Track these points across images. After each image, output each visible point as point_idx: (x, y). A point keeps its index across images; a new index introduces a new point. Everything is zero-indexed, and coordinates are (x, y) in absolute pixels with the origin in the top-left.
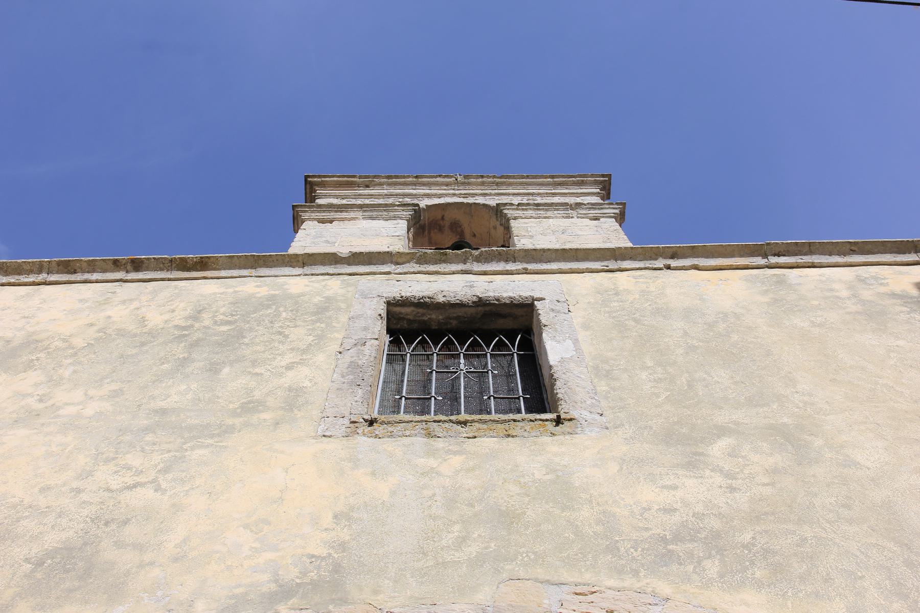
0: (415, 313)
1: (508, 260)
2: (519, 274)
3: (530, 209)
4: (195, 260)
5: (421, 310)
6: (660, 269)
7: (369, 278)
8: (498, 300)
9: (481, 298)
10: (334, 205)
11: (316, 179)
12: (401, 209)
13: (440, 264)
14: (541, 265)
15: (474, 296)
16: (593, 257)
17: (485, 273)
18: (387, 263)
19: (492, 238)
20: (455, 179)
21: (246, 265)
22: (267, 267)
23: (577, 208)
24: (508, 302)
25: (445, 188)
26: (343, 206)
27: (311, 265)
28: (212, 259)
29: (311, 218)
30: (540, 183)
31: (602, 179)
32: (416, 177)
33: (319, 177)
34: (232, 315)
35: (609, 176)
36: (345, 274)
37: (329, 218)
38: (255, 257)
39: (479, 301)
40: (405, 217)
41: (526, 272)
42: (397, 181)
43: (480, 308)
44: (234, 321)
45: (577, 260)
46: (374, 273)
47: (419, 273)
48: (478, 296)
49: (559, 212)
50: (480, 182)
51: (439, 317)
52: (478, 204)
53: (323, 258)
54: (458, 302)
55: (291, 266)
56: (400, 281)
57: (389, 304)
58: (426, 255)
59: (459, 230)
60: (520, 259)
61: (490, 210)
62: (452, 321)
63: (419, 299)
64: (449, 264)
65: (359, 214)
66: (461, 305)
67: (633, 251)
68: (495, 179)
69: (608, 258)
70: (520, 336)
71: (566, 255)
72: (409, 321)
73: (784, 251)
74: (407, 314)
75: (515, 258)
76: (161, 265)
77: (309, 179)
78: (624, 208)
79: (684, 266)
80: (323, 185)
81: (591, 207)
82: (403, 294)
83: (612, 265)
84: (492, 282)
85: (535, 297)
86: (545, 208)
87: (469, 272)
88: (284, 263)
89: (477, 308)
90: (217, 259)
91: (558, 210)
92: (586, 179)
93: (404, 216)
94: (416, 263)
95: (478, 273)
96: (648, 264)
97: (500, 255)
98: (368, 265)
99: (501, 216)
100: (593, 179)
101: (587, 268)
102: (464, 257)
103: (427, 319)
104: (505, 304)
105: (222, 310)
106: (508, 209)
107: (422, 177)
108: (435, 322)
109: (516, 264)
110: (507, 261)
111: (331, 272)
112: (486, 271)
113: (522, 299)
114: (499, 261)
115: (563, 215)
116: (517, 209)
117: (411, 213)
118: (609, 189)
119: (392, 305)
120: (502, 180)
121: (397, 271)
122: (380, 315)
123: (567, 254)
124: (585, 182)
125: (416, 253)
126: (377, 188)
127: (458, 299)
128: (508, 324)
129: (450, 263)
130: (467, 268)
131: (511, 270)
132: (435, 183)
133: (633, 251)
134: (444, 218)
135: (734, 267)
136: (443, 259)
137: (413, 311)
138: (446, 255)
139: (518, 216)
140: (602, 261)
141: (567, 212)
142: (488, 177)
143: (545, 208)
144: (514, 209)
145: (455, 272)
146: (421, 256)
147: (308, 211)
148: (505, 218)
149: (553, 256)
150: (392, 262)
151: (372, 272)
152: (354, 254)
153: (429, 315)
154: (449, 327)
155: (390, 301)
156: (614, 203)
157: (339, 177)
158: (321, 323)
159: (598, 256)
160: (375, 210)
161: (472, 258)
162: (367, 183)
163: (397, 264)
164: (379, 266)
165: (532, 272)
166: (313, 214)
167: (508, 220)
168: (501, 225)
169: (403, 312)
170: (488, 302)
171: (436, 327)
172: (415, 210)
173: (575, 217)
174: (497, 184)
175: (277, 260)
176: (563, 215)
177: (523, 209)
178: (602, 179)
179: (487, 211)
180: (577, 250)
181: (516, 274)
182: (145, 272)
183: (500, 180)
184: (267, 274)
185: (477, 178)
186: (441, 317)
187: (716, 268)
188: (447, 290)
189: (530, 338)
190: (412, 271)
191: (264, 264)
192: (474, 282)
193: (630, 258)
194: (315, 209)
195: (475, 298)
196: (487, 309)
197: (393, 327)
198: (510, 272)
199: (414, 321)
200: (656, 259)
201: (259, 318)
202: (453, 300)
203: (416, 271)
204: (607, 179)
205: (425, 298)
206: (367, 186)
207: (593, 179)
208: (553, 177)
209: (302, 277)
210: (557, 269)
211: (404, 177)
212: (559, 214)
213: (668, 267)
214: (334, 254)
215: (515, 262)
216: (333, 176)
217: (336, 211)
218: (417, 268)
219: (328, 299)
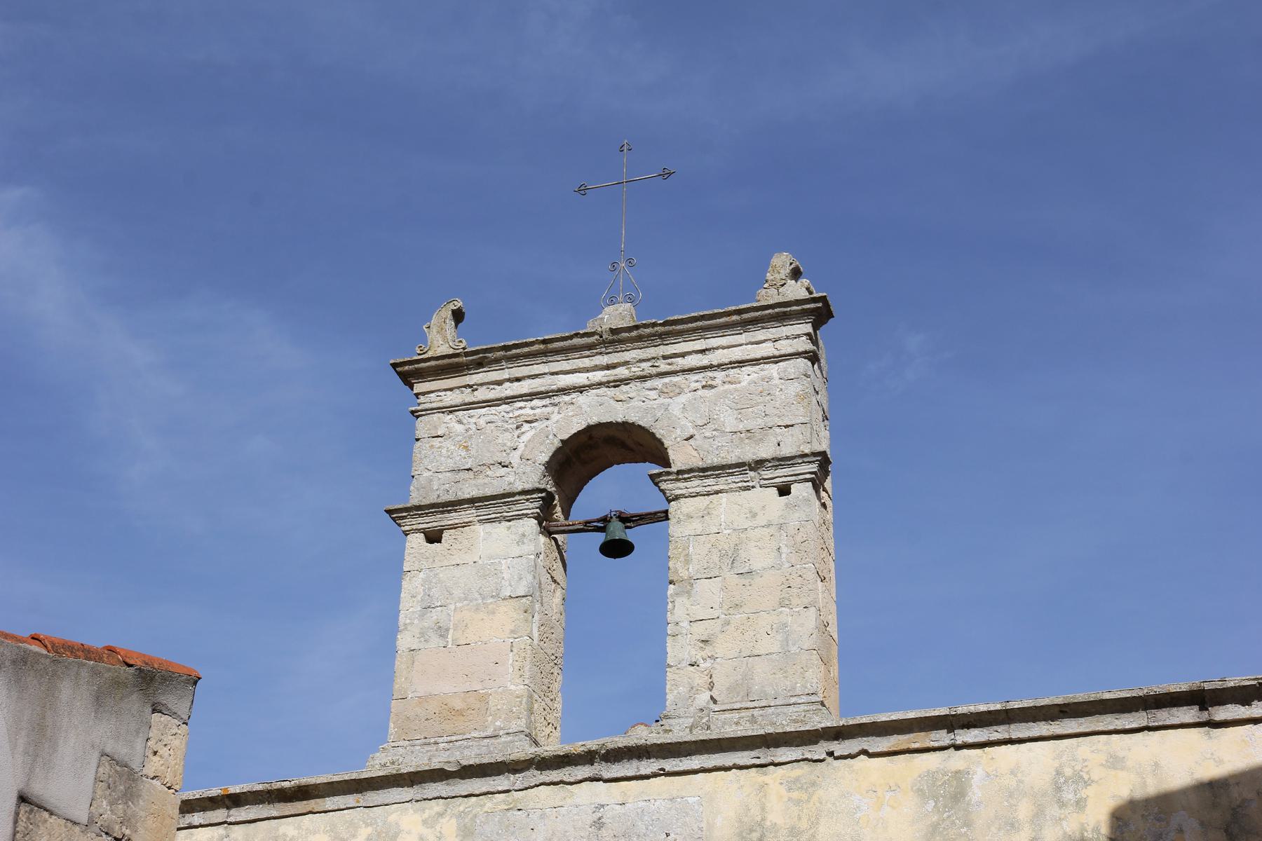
3: (695, 477)
11: (407, 368)
14: (680, 761)
27: (420, 783)
31: (812, 306)
35: (823, 299)
40: (532, 513)
64: (573, 767)
68: (656, 328)
69: (758, 744)
73: (975, 720)
76: (260, 797)
83: (765, 755)
91: (732, 474)
92: (789, 309)
97: (630, 751)
102: (589, 757)
106: (665, 481)
117: (537, 504)
121: (518, 785)
144: (672, 480)
164: (495, 778)
182: (247, 807)
184: (376, 804)
193: (785, 743)
200: (816, 743)
217: (442, 512)
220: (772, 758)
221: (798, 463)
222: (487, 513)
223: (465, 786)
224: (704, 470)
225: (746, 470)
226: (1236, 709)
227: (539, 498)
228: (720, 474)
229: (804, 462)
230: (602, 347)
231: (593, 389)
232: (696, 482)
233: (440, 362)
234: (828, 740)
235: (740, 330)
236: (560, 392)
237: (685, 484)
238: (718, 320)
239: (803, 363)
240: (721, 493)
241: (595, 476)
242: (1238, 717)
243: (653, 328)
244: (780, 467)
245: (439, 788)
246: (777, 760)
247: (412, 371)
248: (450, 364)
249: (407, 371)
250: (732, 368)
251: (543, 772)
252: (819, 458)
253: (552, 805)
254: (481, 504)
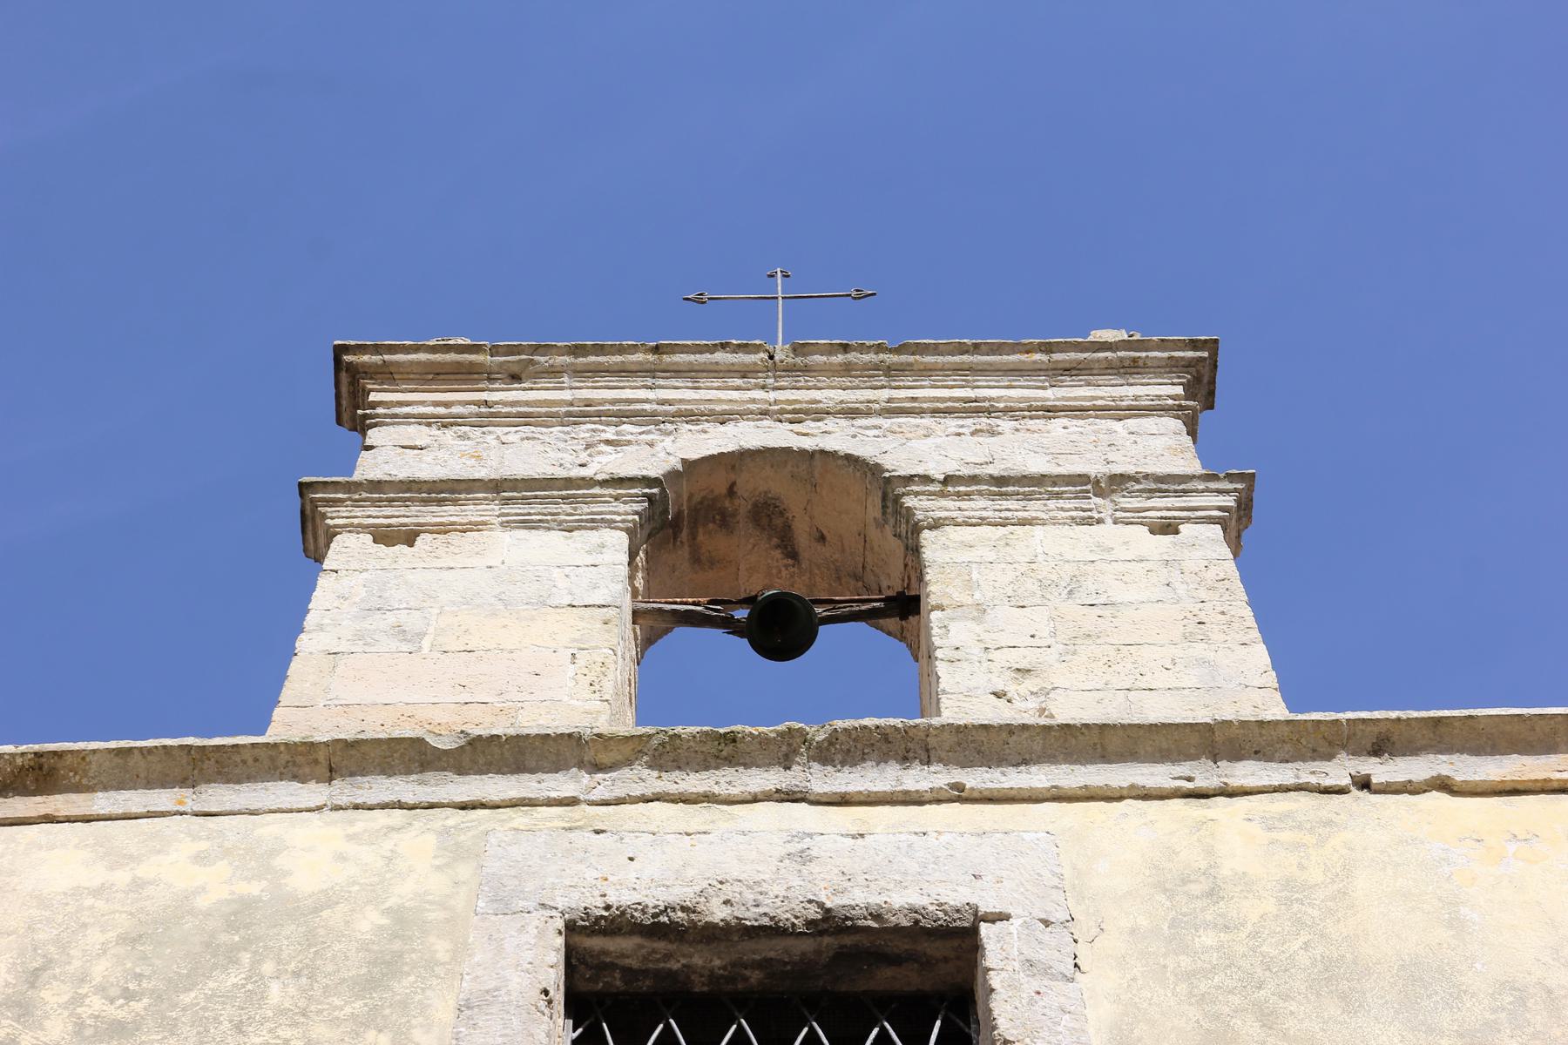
0: (644, 951)
1: (911, 754)
2: (939, 801)
3: (980, 493)
4: (19, 761)
5: (661, 945)
6: (1341, 791)
7: (515, 824)
8: (877, 917)
9: (828, 911)
10: (420, 482)
11: (366, 358)
12: (611, 496)
13: (717, 768)
14: (1003, 774)
15: (810, 901)
16: (1149, 749)
17: (843, 801)
18: (568, 768)
19: (872, 549)
20: (765, 356)
21: (167, 775)
22: (228, 781)
23: (1113, 491)
24: (905, 923)
25: (739, 382)
26: (444, 486)
27: (352, 774)
28: (69, 759)
29: (352, 525)
30: (1011, 367)
31: (1190, 354)
32: (657, 350)
33: (377, 349)
34: (129, 996)
36: (448, 805)
37: (402, 525)
38: (193, 752)
39: (824, 920)
40: (623, 521)
41: (959, 795)
42: (600, 363)
43: (827, 940)
44: (134, 1022)
45: (1103, 757)
46: (531, 803)
47: (657, 798)
48: (821, 905)
49: (1061, 503)
51: (711, 961)
52: (833, 455)
53: (388, 754)
54: (765, 921)
55: (295, 777)
57: (571, 928)
58: (678, 741)
59: (778, 522)
60: (943, 754)
61: (865, 473)
62: (748, 973)
63: (655, 916)
64: (741, 769)
65: (490, 510)
66: (774, 931)
67: (1264, 732)
68: (881, 356)
70: (938, 1023)
71: (1074, 741)
72: (628, 972)
74: (623, 956)
75: (928, 750)
77: (347, 358)
78: (1250, 489)
79: (1410, 781)
80: (389, 375)
81: (1154, 486)
82: (612, 899)
83: (1205, 775)
84: (862, 836)
85: (983, 909)
86: (1021, 490)
87: (799, 796)
88: (276, 768)
89: (819, 939)
90: (83, 758)
91: (1058, 496)
92: (1144, 354)
93: (618, 518)
94: (650, 767)
95: (824, 799)
96: (1306, 772)
98: (512, 773)
99: (897, 512)
100: (1166, 355)
101: (1132, 786)
102: (784, 748)
103: (679, 965)
104: (897, 929)
105: (100, 969)
106: (917, 494)
107: (673, 349)
108: (702, 976)
109: (932, 769)
110: (905, 759)
111: (409, 798)
112: (846, 793)
113: (946, 913)
114: (883, 759)
115: (1074, 514)
116: (942, 495)
117: (638, 507)
118: (1212, 382)
119: (580, 933)
120: (904, 358)
121: (596, 795)
122: (546, 992)
123: (1076, 737)
124: (1141, 363)
125: (650, 736)
126: (543, 383)
127: (765, 914)
128: (907, 979)
129: (746, 766)
130: (794, 782)
131: (917, 791)
132: (712, 368)
133: (1264, 732)
134: (735, 489)
135: (1555, 785)
136: (724, 753)
137: (641, 947)
138: (734, 741)
139: (946, 519)
140: (1174, 761)
141: (1084, 504)
142: (862, 349)
143: (1021, 490)
145: (760, 797)
146: (663, 744)
147: (345, 500)
148: (908, 522)
149: (1037, 746)
150: (581, 765)
151: (525, 799)
152: (474, 739)
153: (684, 956)
154: (740, 986)
155: (574, 922)
156: (1222, 475)
157: (433, 349)
158: (380, 1031)
159: (1165, 745)
160: (536, 497)
161: (808, 749)
162: (515, 369)
163: (597, 768)
164: (545, 776)
165: (976, 795)
166: (358, 512)
167: (917, 529)
168: (895, 536)
169: (612, 949)
170: (849, 923)
171: (705, 989)
172: (650, 498)
173: (1109, 521)
174: (890, 371)
175: (256, 760)
176: (1074, 514)
177: (959, 495)
178: (1190, 354)
179: (858, 474)
180: (1103, 727)
181: (930, 802)
183: (895, 358)
184: (228, 807)
185: (830, 353)
186: (717, 962)
187: (1500, 787)
188: (736, 875)
189: (967, 1030)
190: (638, 793)
191: (219, 773)
192: (810, 835)
193: (1256, 752)
194: (365, 495)
195: (813, 908)
196: (848, 940)
197: (583, 987)
198: (915, 797)
199: (645, 972)
200: (1329, 757)
201: (204, 1009)
202: (751, 916)
203: (649, 792)
204: (1206, 354)
205: (674, 909)
206: (515, 378)
207: (1166, 355)
208: (1048, 348)
209: (328, 815)
210: (1048, 790)
211: (621, 350)
212: (1062, 509)
213: (1364, 784)
214: (418, 742)
215: (928, 763)
216: (416, 349)
217: (425, 502)
218: (653, 782)
219: (403, 922)
220: (1225, 780)
221: (1196, 491)
222: (526, 511)
223: (464, 788)
224: (1001, 481)
225: (1088, 492)
227: (644, 495)
228: (1033, 493)
229: (1207, 490)
230: (768, 377)
231: (748, 420)
232: (981, 503)
233: (438, 357)
234: (1355, 753)
235: (1043, 381)
236: (679, 417)
237: (958, 504)
238: (1005, 357)
239: (1177, 425)
240: (1030, 524)
241: (774, 449)
243: (876, 354)
244: (1158, 494)
245: (396, 788)
246: (1235, 782)
247: (371, 365)
248: (458, 363)
249: (364, 364)
250: (1031, 418)
251: (663, 774)
252: (1239, 486)
253: (682, 828)
254: (515, 494)
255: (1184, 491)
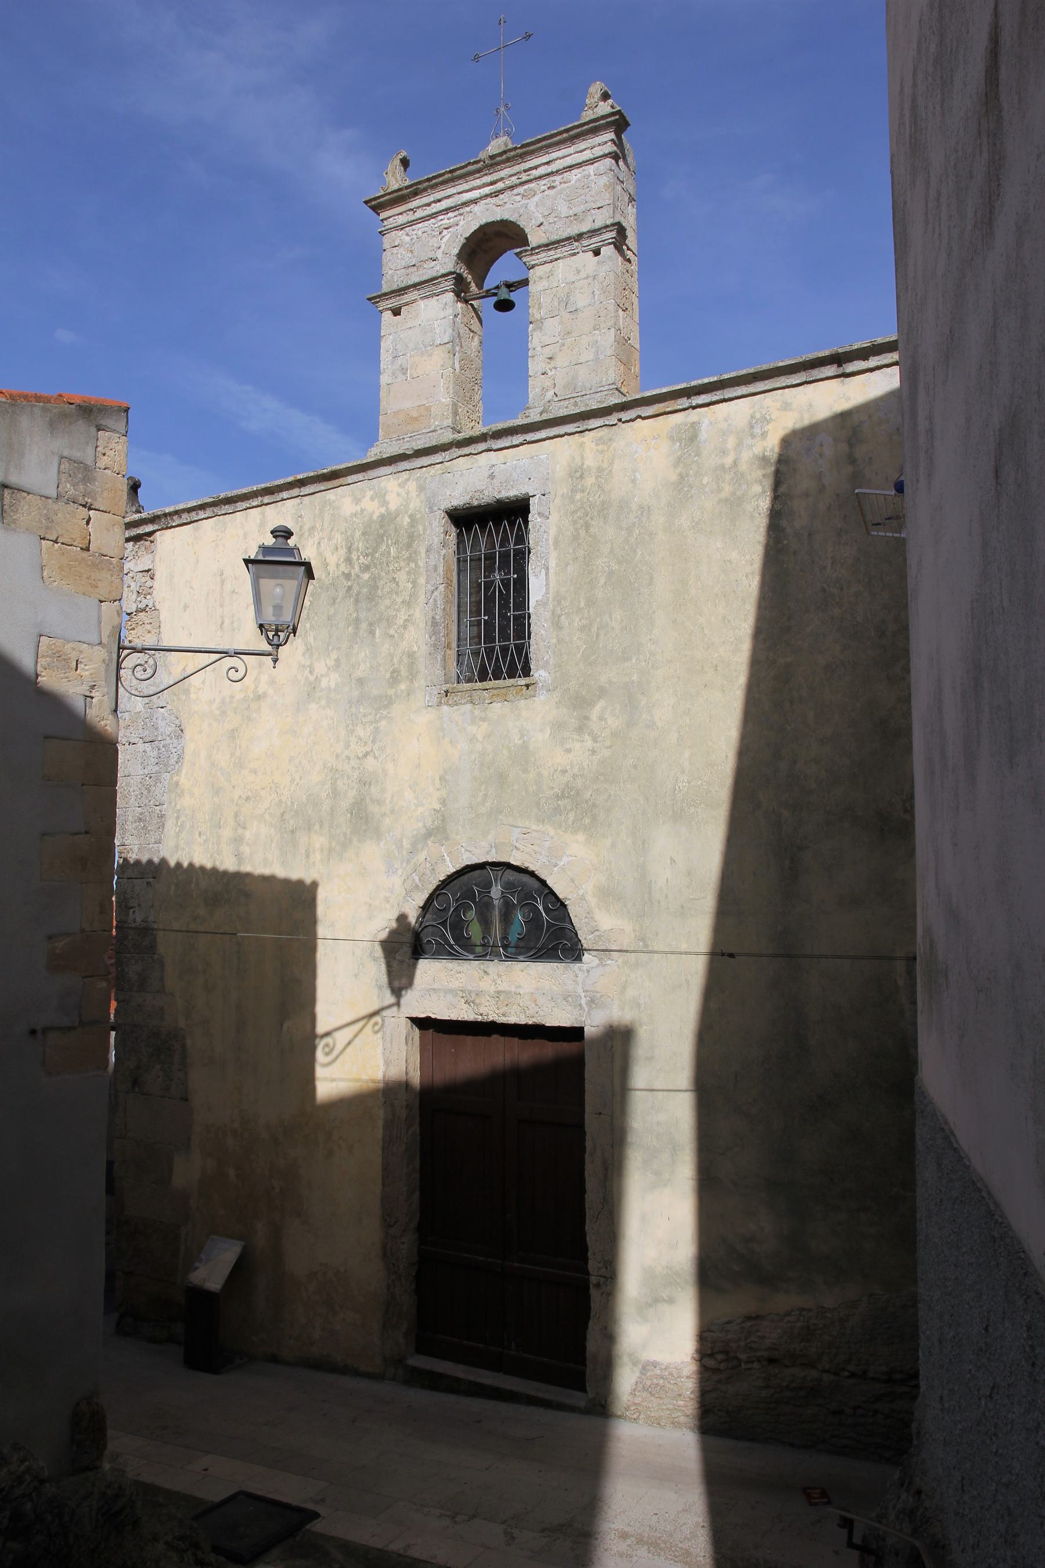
40: (450, 289)
50: (506, 159)
56: (481, 325)
68: (517, 151)
91: (564, 246)
92: (598, 123)
104: (513, 500)
116: (532, 254)
121: (447, 458)
140: (575, 422)
144: (529, 255)
214: (404, 454)
224: (547, 245)
226: (860, 363)
232: (543, 254)
242: (860, 369)
252: (616, 227)
253: (467, 468)
255: (600, 234)
